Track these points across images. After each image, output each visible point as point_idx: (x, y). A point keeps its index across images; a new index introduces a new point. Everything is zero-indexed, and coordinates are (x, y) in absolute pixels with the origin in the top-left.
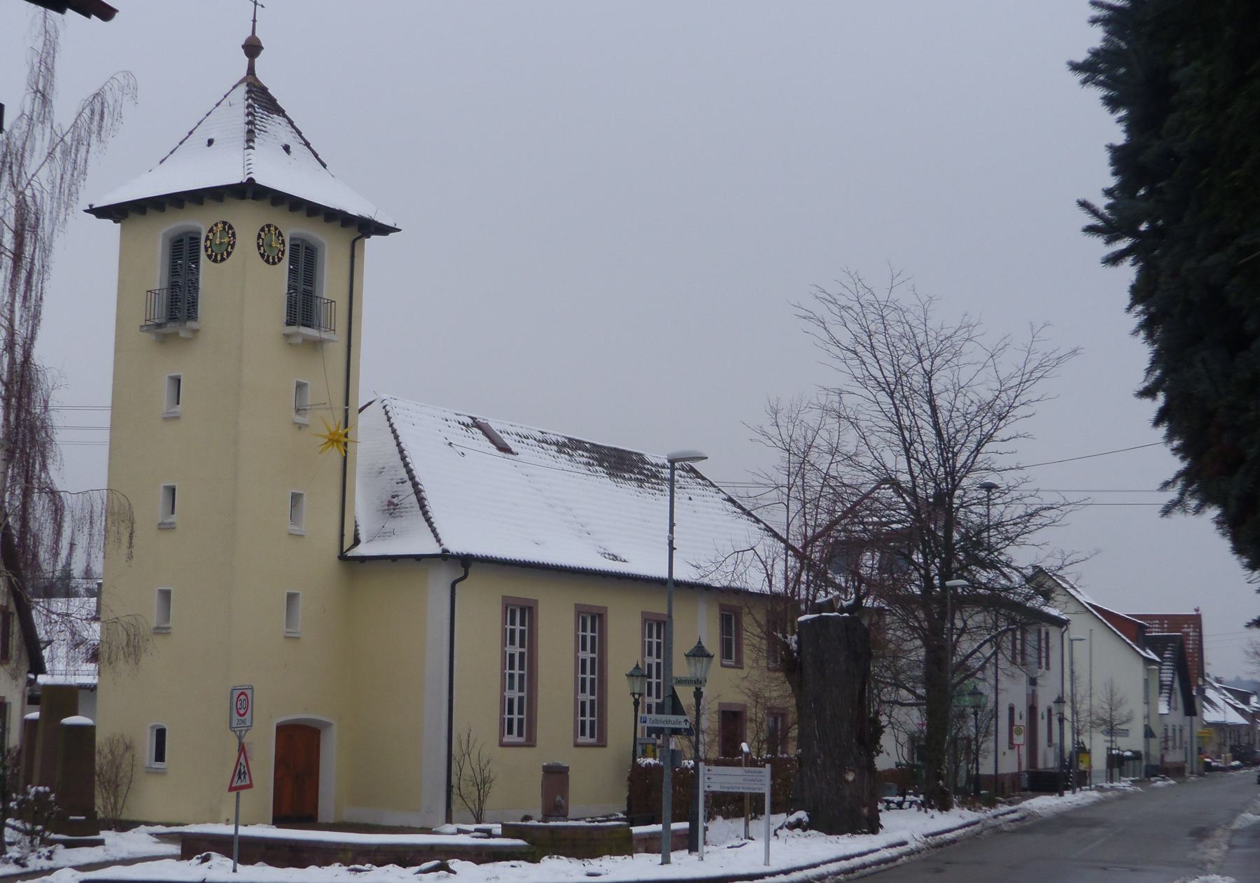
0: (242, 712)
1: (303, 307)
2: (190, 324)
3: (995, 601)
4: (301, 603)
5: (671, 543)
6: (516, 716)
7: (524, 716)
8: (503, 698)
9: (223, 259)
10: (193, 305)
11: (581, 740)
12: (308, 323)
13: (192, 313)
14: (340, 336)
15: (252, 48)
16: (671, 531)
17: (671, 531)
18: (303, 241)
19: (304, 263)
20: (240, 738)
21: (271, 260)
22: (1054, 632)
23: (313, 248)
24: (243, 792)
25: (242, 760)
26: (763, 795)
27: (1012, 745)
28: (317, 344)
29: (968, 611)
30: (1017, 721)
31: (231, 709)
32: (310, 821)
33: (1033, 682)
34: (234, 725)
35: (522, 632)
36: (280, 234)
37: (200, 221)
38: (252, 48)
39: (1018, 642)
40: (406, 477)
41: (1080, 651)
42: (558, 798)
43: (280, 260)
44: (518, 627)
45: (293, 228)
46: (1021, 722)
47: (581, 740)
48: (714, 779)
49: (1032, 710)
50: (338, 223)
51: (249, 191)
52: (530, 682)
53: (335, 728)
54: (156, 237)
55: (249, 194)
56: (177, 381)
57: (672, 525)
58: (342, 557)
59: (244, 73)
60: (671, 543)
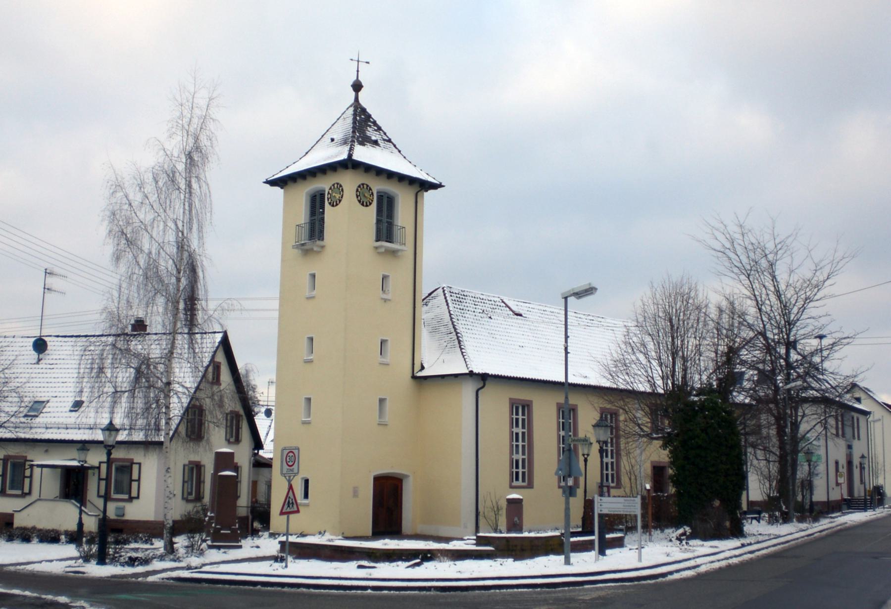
0: (290, 464)
1: (385, 229)
2: (319, 243)
3: (824, 401)
4: (388, 404)
5: (566, 349)
6: (520, 470)
7: (526, 470)
8: (512, 460)
9: (337, 205)
10: (322, 232)
11: (515, 483)
12: (390, 239)
13: (321, 237)
14: (409, 248)
15: (357, 87)
16: (566, 341)
17: (566, 341)
18: (386, 193)
19: (386, 206)
20: (289, 481)
21: (365, 204)
22: (862, 419)
23: (392, 199)
24: (291, 516)
25: (291, 494)
26: (636, 516)
27: (838, 484)
28: (394, 253)
29: (806, 405)
30: (841, 469)
31: (282, 462)
32: (396, 532)
33: (850, 447)
34: (285, 471)
35: (523, 420)
36: (370, 189)
37: (324, 184)
38: (357, 87)
39: (840, 423)
40: (453, 330)
41: (876, 429)
42: (516, 519)
43: (370, 204)
44: (520, 417)
45: (378, 186)
46: (843, 470)
47: (515, 483)
48: (604, 505)
49: (850, 463)
50: (396, 179)
51: (350, 164)
52: (529, 449)
53: (411, 479)
54: (302, 193)
55: (350, 165)
56: (313, 276)
57: (567, 337)
58: (414, 377)
59: (352, 100)
60: (566, 349)
